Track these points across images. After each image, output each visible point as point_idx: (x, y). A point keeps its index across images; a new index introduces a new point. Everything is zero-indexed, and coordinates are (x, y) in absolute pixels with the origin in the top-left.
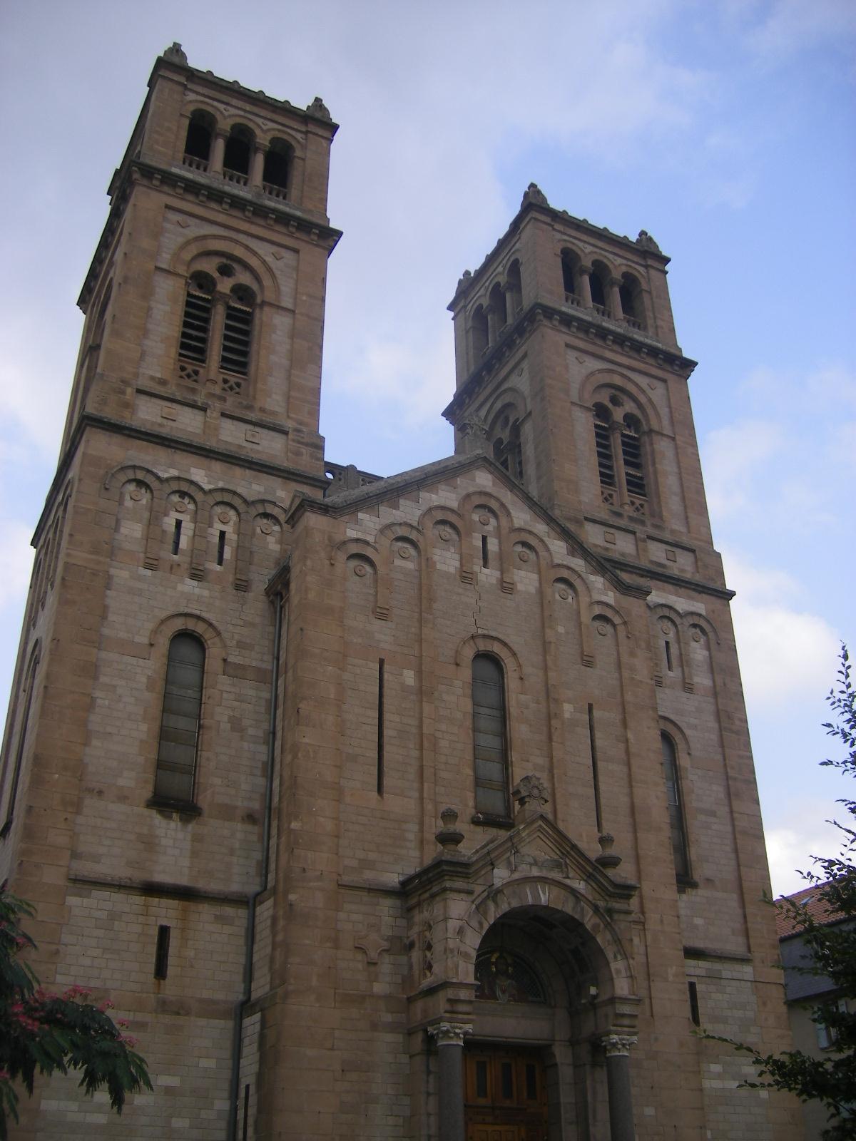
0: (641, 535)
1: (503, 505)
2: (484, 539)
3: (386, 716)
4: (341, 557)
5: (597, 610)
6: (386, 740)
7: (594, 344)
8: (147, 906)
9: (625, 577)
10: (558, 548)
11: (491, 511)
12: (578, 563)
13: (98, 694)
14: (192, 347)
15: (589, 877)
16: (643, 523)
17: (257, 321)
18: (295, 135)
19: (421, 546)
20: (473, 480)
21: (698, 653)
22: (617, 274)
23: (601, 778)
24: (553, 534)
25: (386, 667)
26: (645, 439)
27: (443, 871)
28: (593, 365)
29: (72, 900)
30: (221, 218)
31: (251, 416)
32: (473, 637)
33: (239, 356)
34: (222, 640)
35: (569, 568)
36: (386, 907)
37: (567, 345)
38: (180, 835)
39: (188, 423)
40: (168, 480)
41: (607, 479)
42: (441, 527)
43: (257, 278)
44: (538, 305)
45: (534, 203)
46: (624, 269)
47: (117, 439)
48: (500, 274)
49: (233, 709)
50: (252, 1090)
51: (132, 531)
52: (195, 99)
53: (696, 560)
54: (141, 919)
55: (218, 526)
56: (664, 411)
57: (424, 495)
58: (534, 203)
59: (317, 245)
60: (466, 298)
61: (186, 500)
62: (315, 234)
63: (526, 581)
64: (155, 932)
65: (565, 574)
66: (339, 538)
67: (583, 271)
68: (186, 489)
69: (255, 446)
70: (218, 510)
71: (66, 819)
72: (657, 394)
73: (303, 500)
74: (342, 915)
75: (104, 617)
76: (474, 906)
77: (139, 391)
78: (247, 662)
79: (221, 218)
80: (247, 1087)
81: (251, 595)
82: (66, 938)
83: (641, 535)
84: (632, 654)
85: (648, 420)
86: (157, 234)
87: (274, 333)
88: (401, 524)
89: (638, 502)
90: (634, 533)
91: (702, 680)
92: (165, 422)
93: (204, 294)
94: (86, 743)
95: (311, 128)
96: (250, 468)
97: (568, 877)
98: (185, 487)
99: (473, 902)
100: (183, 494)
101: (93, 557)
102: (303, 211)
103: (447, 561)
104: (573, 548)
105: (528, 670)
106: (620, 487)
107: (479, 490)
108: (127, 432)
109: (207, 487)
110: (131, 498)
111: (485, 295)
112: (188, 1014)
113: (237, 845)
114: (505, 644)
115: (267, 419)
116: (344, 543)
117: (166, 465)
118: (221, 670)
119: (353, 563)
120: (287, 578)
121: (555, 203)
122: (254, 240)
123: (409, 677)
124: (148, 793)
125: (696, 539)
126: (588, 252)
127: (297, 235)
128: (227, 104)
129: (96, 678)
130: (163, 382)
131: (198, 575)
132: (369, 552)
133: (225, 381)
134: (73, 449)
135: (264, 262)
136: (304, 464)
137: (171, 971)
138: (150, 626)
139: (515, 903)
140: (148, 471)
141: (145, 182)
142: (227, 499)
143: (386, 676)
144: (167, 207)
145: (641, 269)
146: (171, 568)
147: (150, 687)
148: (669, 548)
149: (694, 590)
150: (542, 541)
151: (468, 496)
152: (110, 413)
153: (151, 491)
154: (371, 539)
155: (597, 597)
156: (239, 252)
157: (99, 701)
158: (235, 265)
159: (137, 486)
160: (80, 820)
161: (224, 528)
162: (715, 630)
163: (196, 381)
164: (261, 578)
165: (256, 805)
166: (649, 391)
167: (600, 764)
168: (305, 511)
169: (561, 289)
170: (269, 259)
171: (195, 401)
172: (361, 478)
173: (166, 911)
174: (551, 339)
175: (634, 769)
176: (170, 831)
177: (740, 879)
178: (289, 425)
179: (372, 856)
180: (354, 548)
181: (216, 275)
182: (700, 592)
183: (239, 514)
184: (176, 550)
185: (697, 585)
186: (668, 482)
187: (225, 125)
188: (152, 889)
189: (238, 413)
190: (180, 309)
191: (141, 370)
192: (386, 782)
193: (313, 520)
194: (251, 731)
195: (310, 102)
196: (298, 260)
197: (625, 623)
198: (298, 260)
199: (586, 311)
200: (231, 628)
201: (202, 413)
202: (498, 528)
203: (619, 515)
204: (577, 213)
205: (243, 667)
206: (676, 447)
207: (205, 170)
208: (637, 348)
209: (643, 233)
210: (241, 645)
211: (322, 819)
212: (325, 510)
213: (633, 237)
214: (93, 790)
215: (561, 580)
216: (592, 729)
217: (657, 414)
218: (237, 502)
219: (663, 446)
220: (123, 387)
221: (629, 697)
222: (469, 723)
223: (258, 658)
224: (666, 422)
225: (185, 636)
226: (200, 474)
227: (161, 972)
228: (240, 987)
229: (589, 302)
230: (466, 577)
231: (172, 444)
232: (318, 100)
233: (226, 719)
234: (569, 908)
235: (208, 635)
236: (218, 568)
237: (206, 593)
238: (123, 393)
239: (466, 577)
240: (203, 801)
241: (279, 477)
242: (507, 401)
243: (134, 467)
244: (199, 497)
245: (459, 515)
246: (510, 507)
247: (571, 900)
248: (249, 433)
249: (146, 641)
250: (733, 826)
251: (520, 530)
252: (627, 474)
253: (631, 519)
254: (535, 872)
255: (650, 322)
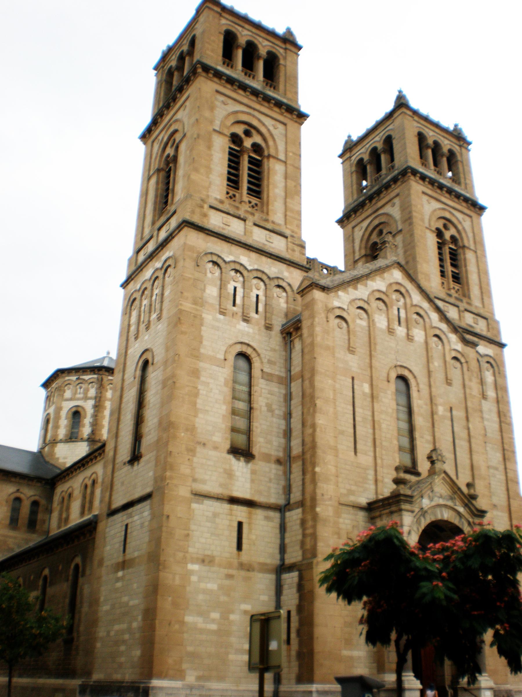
0: (462, 308)
1: (407, 291)
2: (398, 309)
3: (357, 409)
4: (332, 317)
5: (454, 354)
6: (357, 423)
7: (436, 192)
8: (231, 510)
9: (468, 337)
10: (434, 316)
11: (401, 293)
12: (444, 326)
13: (200, 387)
14: (233, 181)
15: (466, 506)
16: (461, 301)
17: (266, 167)
18: (280, 51)
19: (369, 311)
20: (392, 275)
21: (489, 377)
22: (445, 150)
23: (457, 449)
24: (431, 309)
25: (356, 381)
26: (460, 251)
27: (401, 499)
28: (436, 205)
29: (194, 506)
30: (245, 101)
31: (269, 226)
32: (395, 366)
33: (257, 188)
34: (261, 359)
35: (440, 329)
36: (361, 515)
37: (424, 193)
38: (245, 470)
39: (236, 228)
40: (229, 262)
41: (443, 274)
42: (378, 302)
43: (265, 139)
44: (409, 167)
45: (401, 103)
46: (449, 147)
47: (202, 235)
48: (377, 141)
49: (268, 399)
50: (294, 614)
51: (212, 292)
52: (225, 23)
53: (488, 325)
54: (229, 517)
55: (255, 292)
56: (470, 235)
57: (369, 283)
58: (401, 103)
59: (296, 122)
60: (351, 151)
61: (238, 275)
62: (295, 114)
63: (419, 334)
64: (236, 525)
65: (438, 332)
66: (330, 306)
67: (428, 147)
68: (239, 270)
69: (271, 244)
70: (255, 281)
71: (189, 459)
72: (466, 224)
73: (312, 283)
74: (341, 520)
75: (201, 342)
76: (415, 520)
77: (211, 207)
78: (273, 372)
79: (245, 101)
80: (289, 612)
81: (273, 333)
82: (193, 527)
83: (462, 308)
84: (470, 380)
85: (462, 239)
86: (212, 108)
87: (275, 174)
88: (359, 299)
89: (456, 288)
90: (457, 306)
91: (491, 393)
92: (224, 226)
93: (236, 146)
94: (196, 416)
95: (288, 46)
96: (270, 258)
97: (456, 505)
98: (238, 267)
99: (414, 517)
100: (237, 271)
101: (194, 306)
102: (288, 99)
103: (381, 321)
104: (442, 318)
105: (422, 386)
106: (448, 279)
107: (396, 281)
108: (207, 232)
109: (249, 268)
110: (210, 272)
111: (365, 153)
112: (253, 570)
113: (273, 477)
114: (410, 371)
115: (277, 228)
116: (333, 309)
117: (229, 253)
118: (260, 376)
119: (338, 320)
120: (299, 325)
121: (414, 104)
122: (263, 116)
123: (366, 388)
124: (228, 446)
125: (487, 312)
126: (431, 136)
127: (285, 114)
128: (243, 27)
129: (198, 378)
130: (222, 202)
131: (246, 319)
132: (345, 315)
133: (250, 202)
134: (170, 238)
135: (269, 130)
136: (296, 257)
137: (244, 546)
138: (224, 349)
139: (433, 519)
140: (219, 256)
141: (204, 74)
142: (261, 276)
143: (355, 387)
144: (217, 91)
145: (282, 51)
146: (233, 315)
147: (226, 384)
148: (475, 316)
149: (488, 342)
150: (426, 313)
151: (390, 285)
152: (196, 219)
153: (221, 269)
154: (345, 307)
155: (454, 347)
156: (255, 123)
157: (201, 392)
158: (253, 131)
159: (213, 265)
160: (195, 460)
161: (258, 292)
162: (498, 366)
163: (234, 201)
164: (278, 322)
165: (281, 454)
166: (463, 223)
167: (457, 441)
168: (313, 289)
169: (418, 157)
170: (271, 128)
171: (240, 215)
172: (321, 265)
173: (241, 513)
174: (416, 187)
175: (473, 445)
176: (239, 466)
177: (509, 506)
178: (288, 232)
179: (354, 488)
180: (338, 312)
181: (243, 136)
182: (491, 343)
183: (265, 285)
184: (234, 304)
185: (489, 339)
186: (473, 278)
187: (242, 40)
188: (233, 501)
189: (262, 224)
190: (227, 156)
191: (210, 194)
192: (358, 446)
193: (317, 294)
194: (277, 412)
195: (285, 30)
196: (286, 130)
197: (467, 362)
198: (286, 130)
199: (237, 72)
200: (264, 352)
201: (243, 222)
202: (405, 304)
203: (450, 295)
204: (424, 111)
205: (271, 375)
206: (477, 257)
207: (253, 78)
208: (458, 196)
209: (456, 126)
210: (270, 362)
211: (330, 467)
212: (324, 289)
213: (451, 128)
214: (200, 443)
215: (436, 336)
216: (452, 420)
217: (467, 236)
218: (265, 278)
219: (470, 256)
220: (202, 203)
221: (469, 404)
222: (395, 415)
223: (278, 370)
224: (472, 242)
225: (242, 355)
226: (247, 260)
227: (239, 547)
228: (278, 556)
229: (432, 167)
230: (390, 331)
231: (231, 241)
232: (400, 92)
233: (264, 404)
234: (456, 521)
235: (253, 355)
236: (256, 316)
237: (251, 331)
238: (202, 207)
239: (390, 331)
240: (255, 451)
241: (285, 264)
242: (382, 220)
243: (212, 253)
244: (245, 273)
245: (387, 296)
246: (410, 291)
247: (458, 518)
248: (268, 236)
249: (222, 357)
250: (506, 476)
251: (416, 306)
252: (452, 271)
253: (457, 299)
254: (441, 502)
255: (462, 180)
